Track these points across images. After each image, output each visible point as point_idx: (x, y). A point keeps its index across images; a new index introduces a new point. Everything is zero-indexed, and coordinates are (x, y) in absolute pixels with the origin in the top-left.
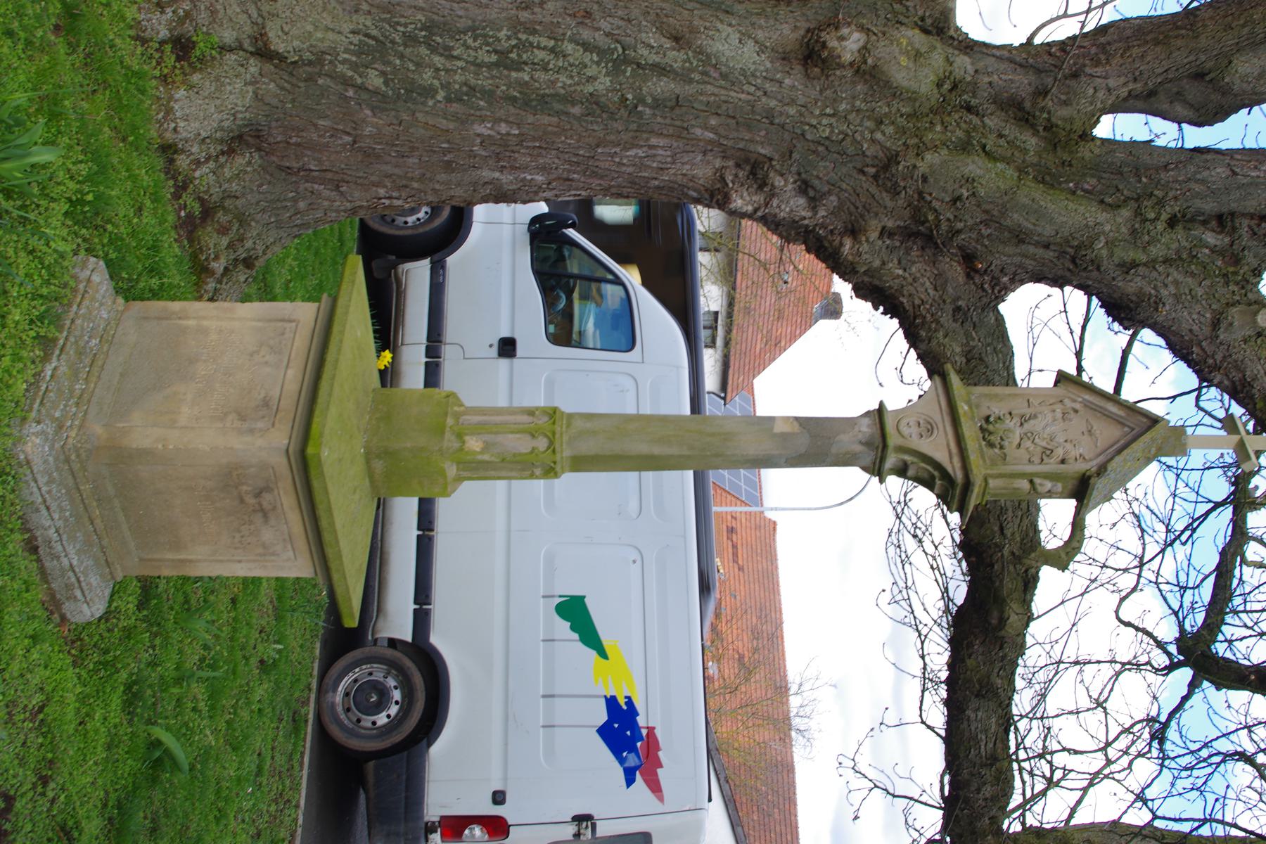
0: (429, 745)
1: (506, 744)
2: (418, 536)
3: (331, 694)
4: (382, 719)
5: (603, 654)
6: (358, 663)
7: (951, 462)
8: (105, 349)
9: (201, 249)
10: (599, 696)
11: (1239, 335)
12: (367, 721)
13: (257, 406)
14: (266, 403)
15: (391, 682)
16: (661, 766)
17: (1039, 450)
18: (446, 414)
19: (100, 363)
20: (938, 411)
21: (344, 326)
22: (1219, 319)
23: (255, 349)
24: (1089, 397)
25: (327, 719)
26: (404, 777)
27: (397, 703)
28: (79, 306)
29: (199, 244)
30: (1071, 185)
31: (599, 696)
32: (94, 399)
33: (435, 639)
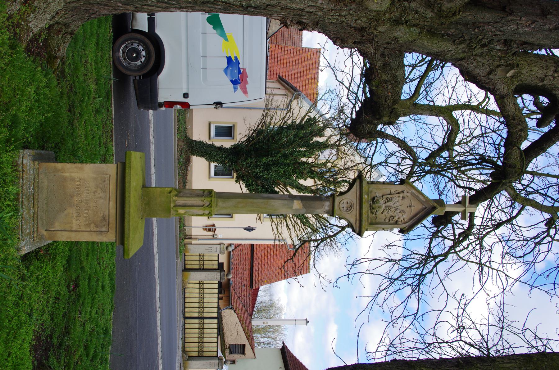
0: (158, 74)
1: (188, 75)
2: (148, 18)
3: (117, 53)
4: (139, 63)
5: (227, 40)
6: (127, 40)
7: (356, 224)
8: (36, 190)
9: (52, 50)
10: (224, 57)
11: (497, 77)
12: (133, 63)
13: (101, 220)
14: (104, 219)
15: (141, 48)
16: (248, 84)
17: (389, 216)
18: (170, 202)
22: (491, 72)
24: (413, 191)
25: (117, 63)
26: (149, 87)
27: (144, 56)
28: (22, 179)
29: (50, 48)
30: (443, 32)
31: (224, 57)
32: (39, 217)
33: (157, 32)
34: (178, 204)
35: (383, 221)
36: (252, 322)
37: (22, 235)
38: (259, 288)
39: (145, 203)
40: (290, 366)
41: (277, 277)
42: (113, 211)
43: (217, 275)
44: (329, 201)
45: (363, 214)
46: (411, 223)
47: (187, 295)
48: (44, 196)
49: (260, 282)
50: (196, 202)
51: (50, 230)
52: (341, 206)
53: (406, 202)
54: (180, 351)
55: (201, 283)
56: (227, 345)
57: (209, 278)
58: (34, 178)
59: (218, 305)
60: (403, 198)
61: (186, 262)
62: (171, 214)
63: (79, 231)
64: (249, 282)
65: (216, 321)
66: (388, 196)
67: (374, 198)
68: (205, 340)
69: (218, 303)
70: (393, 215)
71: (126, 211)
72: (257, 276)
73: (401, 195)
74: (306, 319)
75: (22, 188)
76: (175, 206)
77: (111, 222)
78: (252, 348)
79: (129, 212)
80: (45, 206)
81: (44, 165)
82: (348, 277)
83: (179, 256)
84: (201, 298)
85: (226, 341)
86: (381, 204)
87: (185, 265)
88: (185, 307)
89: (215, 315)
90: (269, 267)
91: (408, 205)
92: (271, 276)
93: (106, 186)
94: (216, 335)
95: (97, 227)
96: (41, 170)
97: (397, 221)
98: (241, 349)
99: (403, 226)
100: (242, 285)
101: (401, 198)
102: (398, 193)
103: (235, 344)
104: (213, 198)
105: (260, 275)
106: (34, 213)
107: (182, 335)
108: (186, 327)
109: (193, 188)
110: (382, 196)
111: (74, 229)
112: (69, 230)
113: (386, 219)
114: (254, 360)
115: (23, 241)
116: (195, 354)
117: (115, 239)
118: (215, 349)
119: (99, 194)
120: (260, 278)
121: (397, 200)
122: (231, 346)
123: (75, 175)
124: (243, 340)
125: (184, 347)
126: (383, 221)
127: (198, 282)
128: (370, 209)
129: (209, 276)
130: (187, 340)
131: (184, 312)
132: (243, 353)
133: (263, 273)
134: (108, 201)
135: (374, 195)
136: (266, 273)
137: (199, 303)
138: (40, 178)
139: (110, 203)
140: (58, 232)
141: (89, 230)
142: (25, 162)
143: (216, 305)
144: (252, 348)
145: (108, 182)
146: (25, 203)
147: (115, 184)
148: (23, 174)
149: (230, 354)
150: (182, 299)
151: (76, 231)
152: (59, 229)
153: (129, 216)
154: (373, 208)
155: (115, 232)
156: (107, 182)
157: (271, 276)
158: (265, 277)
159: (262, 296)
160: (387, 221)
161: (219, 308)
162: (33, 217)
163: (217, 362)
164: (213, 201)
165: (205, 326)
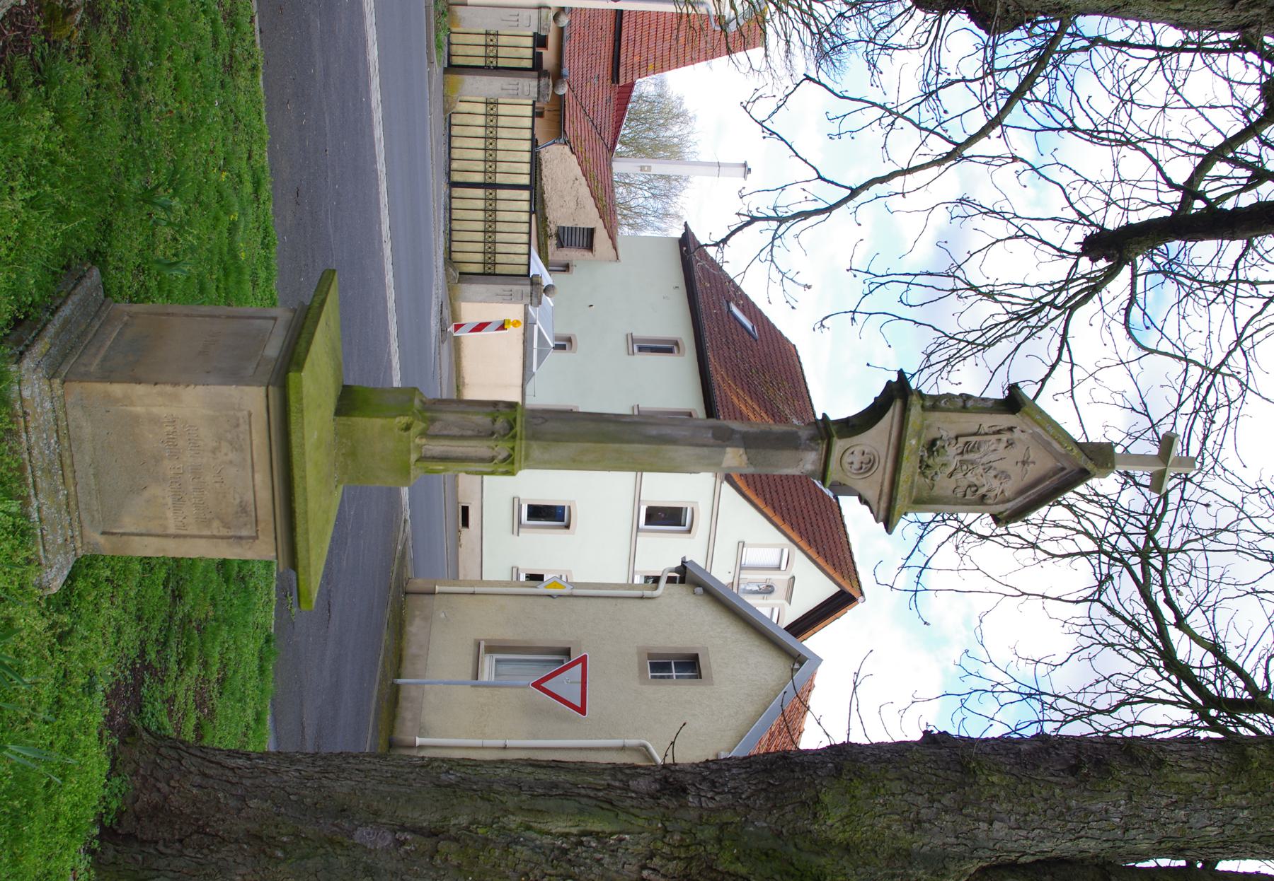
13: (237, 513)
14: (243, 509)
17: (965, 483)
18: (409, 452)
19: (68, 462)
20: (886, 444)
21: (304, 471)
23: (215, 444)
28: (27, 432)
32: (82, 506)
34: (429, 454)
35: (949, 492)
36: (614, 165)
37: (46, 557)
38: (633, 84)
39: (344, 451)
40: (698, 285)
41: (681, 56)
42: (264, 495)
43: (529, 85)
44: (816, 450)
45: (901, 483)
46: (1020, 501)
47: (455, 130)
48: (87, 459)
49: (636, 67)
50: (473, 449)
51: (113, 534)
52: (847, 459)
53: (1017, 453)
54: (441, 262)
55: (491, 103)
56: (553, 228)
57: (511, 92)
58: (56, 419)
59: (533, 135)
60: (1010, 444)
61: (454, 48)
62: (412, 477)
63: (185, 536)
64: (610, 69)
65: (525, 194)
66: (969, 439)
67: (933, 443)
68: (499, 237)
69: (532, 129)
70: (977, 483)
71: (297, 510)
72: (630, 54)
73: (1005, 437)
74: (745, 165)
75: (30, 454)
76: (422, 459)
77: (260, 517)
78: (610, 237)
79: (306, 512)
80: (92, 482)
81: (76, 388)
82: (853, 319)
83: (435, 59)
84: (491, 138)
85: (550, 218)
86: (950, 458)
87: (450, 55)
88: (450, 159)
89: (525, 180)
90: (660, 30)
91: (1020, 459)
92: (666, 53)
93: (242, 436)
94: (525, 217)
95: (229, 528)
96: (70, 400)
97: (984, 496)
98: (587, 239)
99: (1000, 508)
100: (591, 78)
101: (1003, 445)
102: (999, 432)
103: (570, 225)
104: (518, 442)
105: (637, 51)
106: (67, 496)
107: (445, 225)
108: (453, 206)
109: (471, 394)
110: (957, 438)
111: (172, 530)
112: (160, 533)
113: (958, 490)
114: (615, 265)
115: (51, 567)
116: (477, 268)
117: (274, 554)
118: (524, 259)
119: (226, 454)
120: (636, 59)
121: (993, 447)
122: (561, 231)
123: (162, 411)
124: (589, 217)
125: (449, 252)
126: (949, 492)
127: (484, 100)
128: (920, 467)
129: (511, 87)
130: (456, 236)
131: (449, 172)
132: (590, 246)
133: (645, 45)
134: (250, 470)
135: (933, 434)
136: (652, 45)
137: (485, 149)
138: (70, 419)
139: (257, 476)
140: (132, 538)
141: (208, 533)
142: (26, 393)
143: (528, 134)
144: (612, 238)
145: (247, 427)
146: (43, 484)
147: (265, 434)
148: (25, 422)
149: (558, 248)
150: (444, 139)
151: (176, 536)
152: (135, 531)
153: (307, 522)
154: (928, 466)
155: (273, 541)
156: (244, 427)
157: (666, 53)
158: (651, 57)
159: (645, 86)
160: (960, 495)
161: (534, 142)
162: (68, 505)
163: (528, 289)
164: (516, 449)
165: (500, 205)
